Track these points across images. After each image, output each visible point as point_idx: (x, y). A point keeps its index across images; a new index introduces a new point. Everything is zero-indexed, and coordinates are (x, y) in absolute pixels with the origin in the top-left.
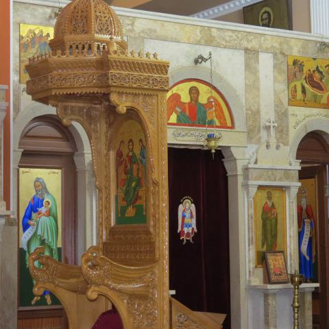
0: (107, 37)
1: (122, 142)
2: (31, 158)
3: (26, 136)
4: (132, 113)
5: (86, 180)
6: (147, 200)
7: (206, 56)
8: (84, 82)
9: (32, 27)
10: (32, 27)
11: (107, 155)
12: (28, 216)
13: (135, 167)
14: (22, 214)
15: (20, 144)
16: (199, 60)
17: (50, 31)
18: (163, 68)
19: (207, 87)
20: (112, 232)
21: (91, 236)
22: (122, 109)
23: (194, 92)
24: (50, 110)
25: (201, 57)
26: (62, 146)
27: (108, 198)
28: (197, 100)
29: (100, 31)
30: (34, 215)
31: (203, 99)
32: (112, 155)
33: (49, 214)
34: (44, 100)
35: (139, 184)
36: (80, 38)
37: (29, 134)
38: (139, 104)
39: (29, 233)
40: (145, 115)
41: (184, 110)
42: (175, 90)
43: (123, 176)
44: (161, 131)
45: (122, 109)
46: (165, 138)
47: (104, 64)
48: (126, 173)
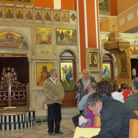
0: (118, 38)
1: (122, 57)
2: (105, 61)
3: (103, 58)
4: (124, 51)
5: (115, 65)
6: (127, 67)
7: (137, 41)
8: (114, 46)
9: (103, 38)
10: (103, 38)
11: (119, 60)
12: (104, 72)
13: (124, 62)
14: (103, 72)
15: (102, 59)
16: (135, 42)
17: (107, 39)
18: (129, 43)
19: (97, 126)
20: (120, 74)
21: (116, 74)
22: (122, 51)
23: (134, 48)
24: (108, 52)
25: (136, 41)
26: (110, 59)
27: (119, 68)
28: (135, 50)
29: (117, 37)
30: (105, 72)
31: (136, 49)
32: (120, 60)
33: (108, 72)
34: (107, 50)
35: (125, 65)
36: (113, 38)
37: (104, 57)
38: (125, 50)
39: (105, 75)
40: (126, 52)
41: (133, 52)
42: (131, 48)
43: (122, 63)
44: (129, 57)
45: (122, 51)
46: (130, 57)
47: (118, 43)
48: (123, 63)
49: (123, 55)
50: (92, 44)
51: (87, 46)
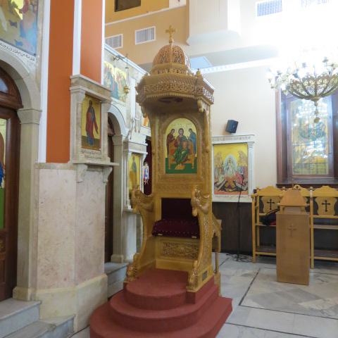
49: (183, 126)
50: (91, 67)
51: (76, 70)
